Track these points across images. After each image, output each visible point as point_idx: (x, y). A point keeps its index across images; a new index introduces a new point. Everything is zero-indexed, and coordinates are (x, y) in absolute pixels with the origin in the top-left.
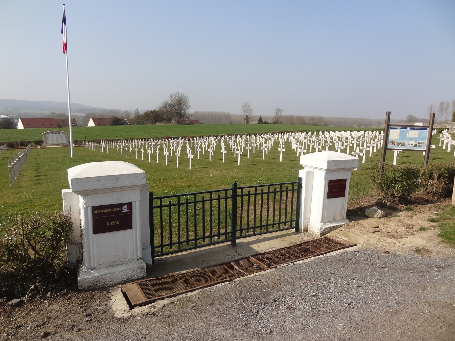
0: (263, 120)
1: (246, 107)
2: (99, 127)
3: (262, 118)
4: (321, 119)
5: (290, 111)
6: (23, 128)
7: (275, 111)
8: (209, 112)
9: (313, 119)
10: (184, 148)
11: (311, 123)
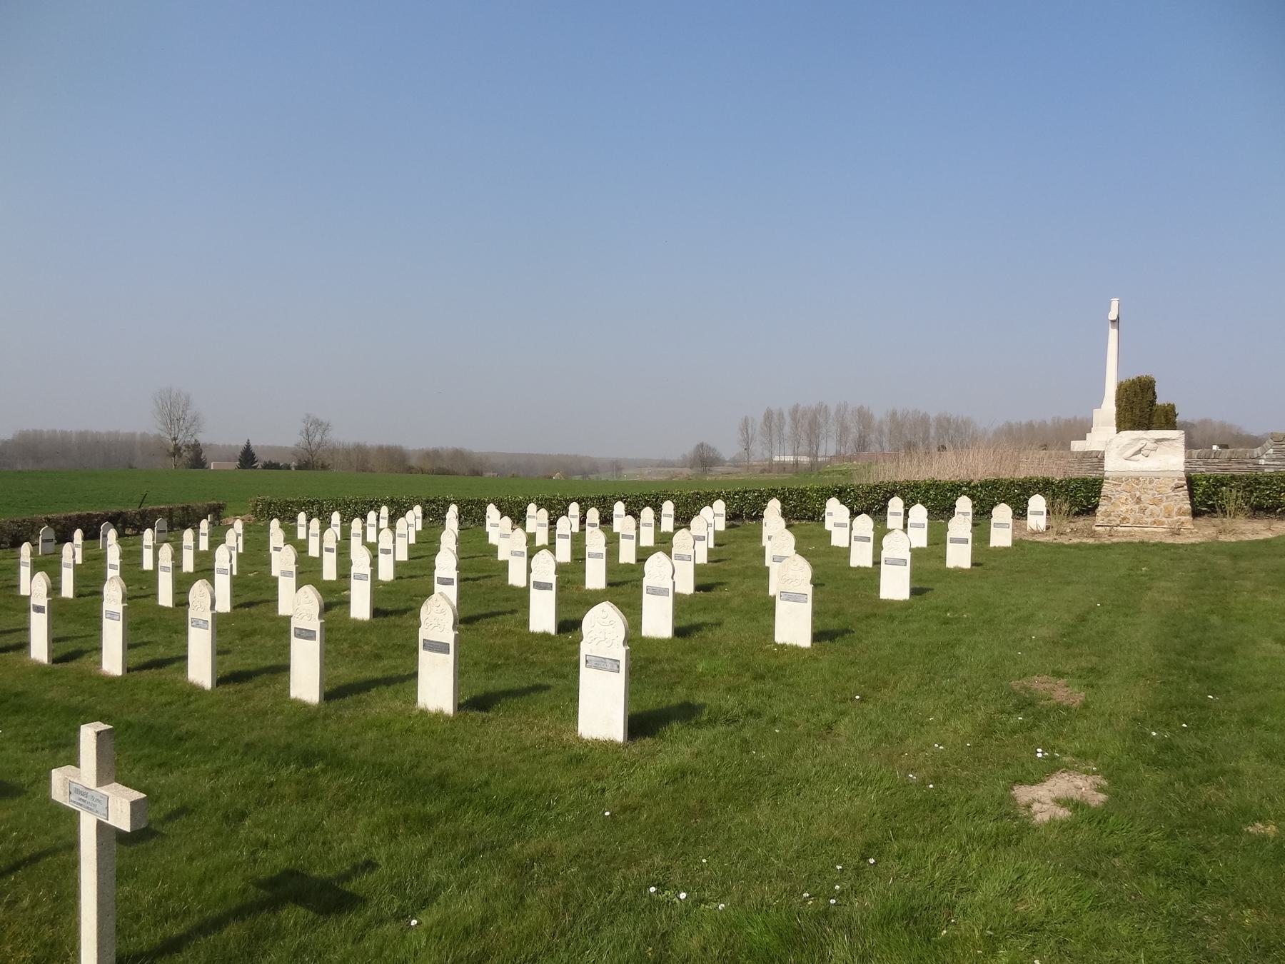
0: (258, 455)
1: (174, 410)
2: (679, 640)
3: (253, 449)
4: (458, 455)
5: (354, 427)
6: (449, 708)
7: (302, 426)
8: (82, 435)
9: (434, 455)
10: (254, 590)
11: (428, 466)
